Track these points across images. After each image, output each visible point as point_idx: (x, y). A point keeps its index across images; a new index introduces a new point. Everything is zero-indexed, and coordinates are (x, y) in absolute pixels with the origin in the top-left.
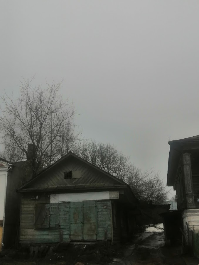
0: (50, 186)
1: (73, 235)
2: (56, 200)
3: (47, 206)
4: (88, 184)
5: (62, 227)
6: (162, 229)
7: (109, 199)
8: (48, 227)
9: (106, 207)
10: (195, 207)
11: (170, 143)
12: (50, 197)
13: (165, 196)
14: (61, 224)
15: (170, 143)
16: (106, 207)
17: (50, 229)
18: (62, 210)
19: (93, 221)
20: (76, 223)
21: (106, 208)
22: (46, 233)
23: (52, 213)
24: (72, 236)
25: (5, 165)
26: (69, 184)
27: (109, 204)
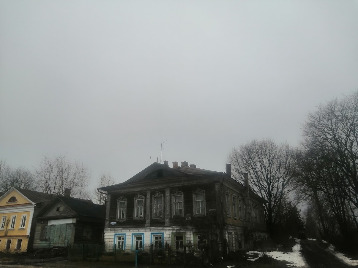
0: (50, 216)
1: (55, 244)
2: (52, 223)
3: (46, 227)
4: (66, 214)
5: (51, 239)
6: (137, 216)
7: (72, 223)
8: (45, 239)
9: (70, 227)
10: (108, 227)
11: (173, 163)
12: (48, 222)
13: (316, 116)
14: (50, 237)
15: (173, 163)
16: (70, 227)
17: (46, 240)
18: (52, 229)
19: (64, 235)
20: (57, 237)
21: (71, 228)
22: (44, 242)
23: (47, 231)
24: (54, 244)
25: (33, 204)
26: (58, 214)
27: (72, 226)
